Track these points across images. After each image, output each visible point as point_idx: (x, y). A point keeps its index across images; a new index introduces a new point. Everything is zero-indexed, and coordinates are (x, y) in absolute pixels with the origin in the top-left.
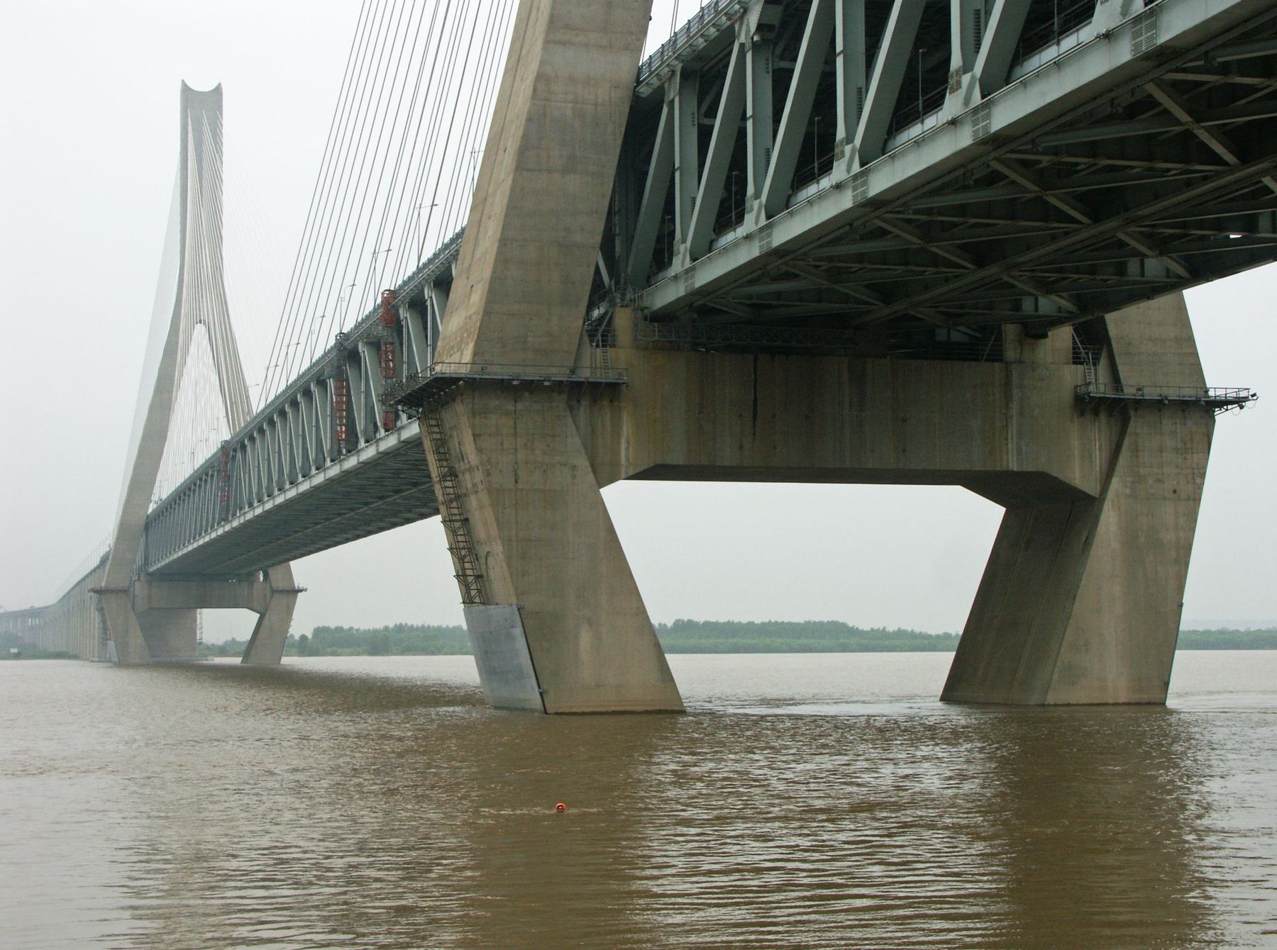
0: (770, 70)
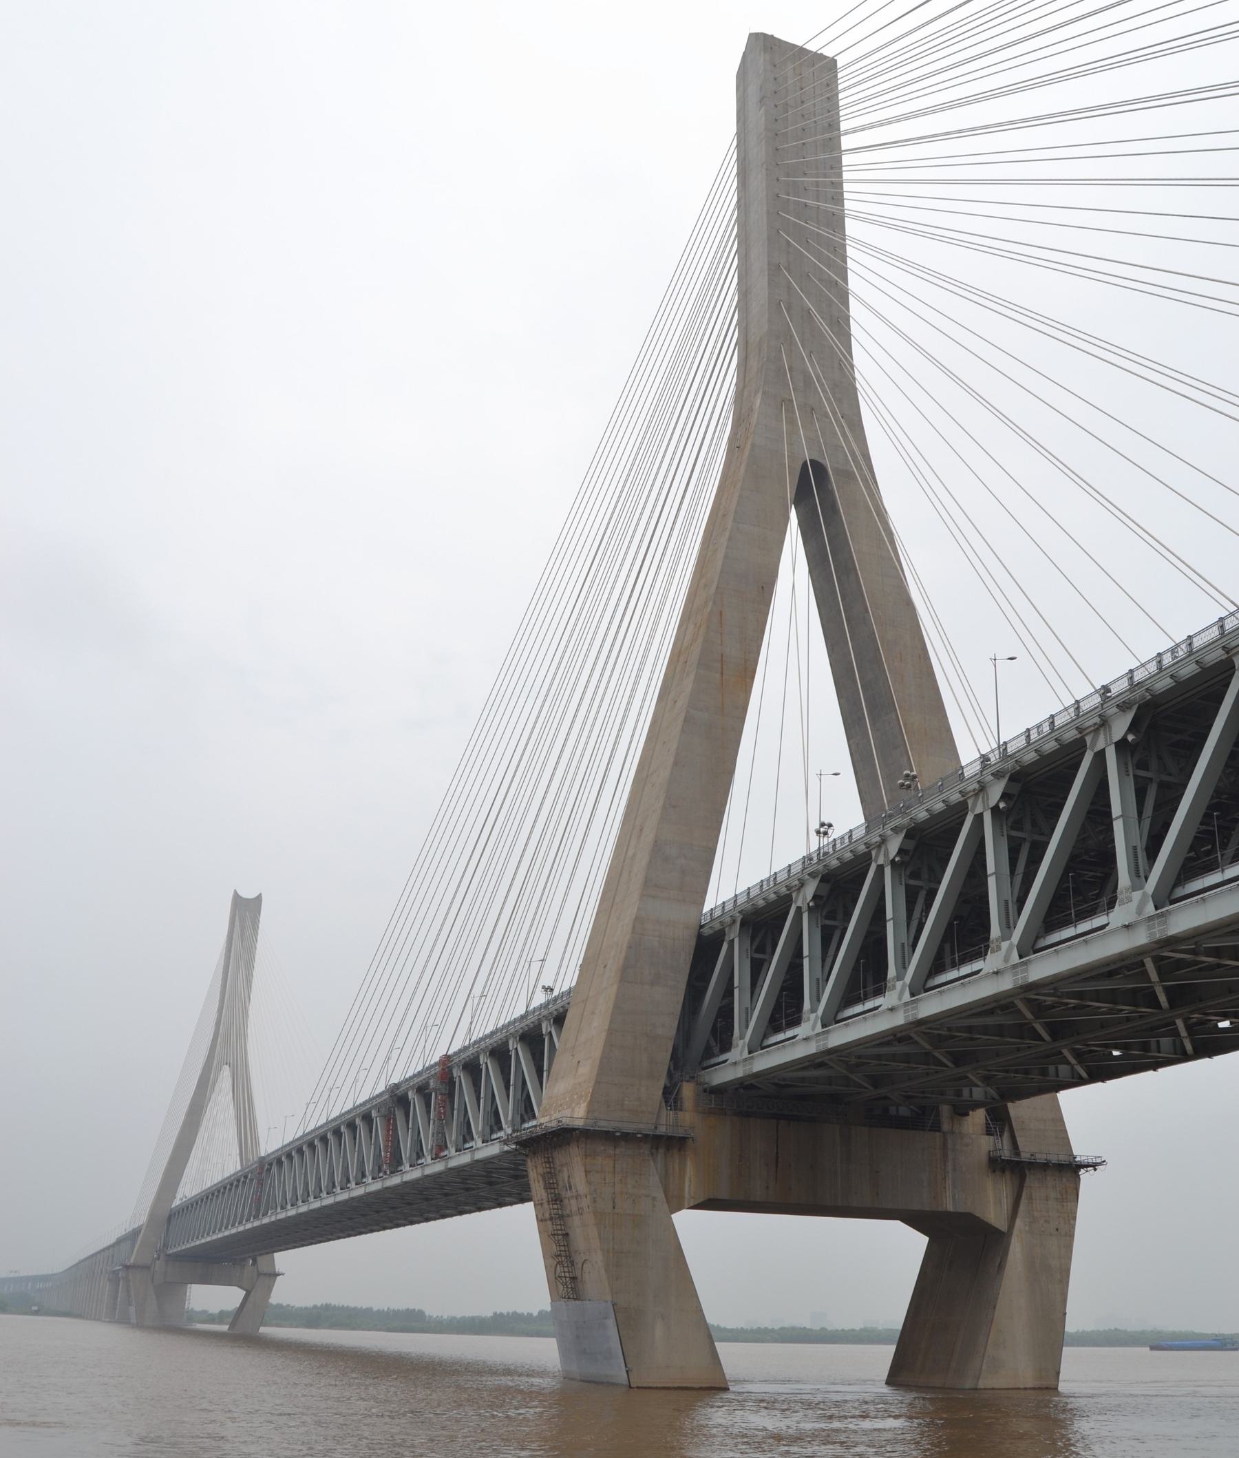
0: (819, 925)
